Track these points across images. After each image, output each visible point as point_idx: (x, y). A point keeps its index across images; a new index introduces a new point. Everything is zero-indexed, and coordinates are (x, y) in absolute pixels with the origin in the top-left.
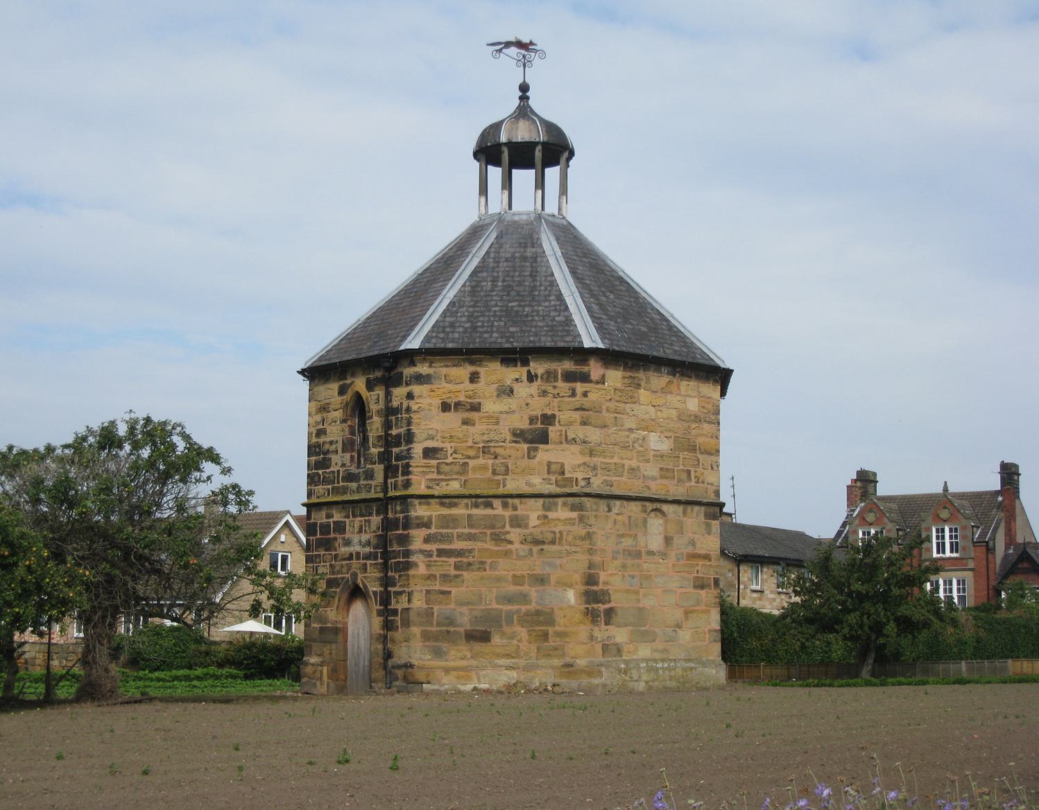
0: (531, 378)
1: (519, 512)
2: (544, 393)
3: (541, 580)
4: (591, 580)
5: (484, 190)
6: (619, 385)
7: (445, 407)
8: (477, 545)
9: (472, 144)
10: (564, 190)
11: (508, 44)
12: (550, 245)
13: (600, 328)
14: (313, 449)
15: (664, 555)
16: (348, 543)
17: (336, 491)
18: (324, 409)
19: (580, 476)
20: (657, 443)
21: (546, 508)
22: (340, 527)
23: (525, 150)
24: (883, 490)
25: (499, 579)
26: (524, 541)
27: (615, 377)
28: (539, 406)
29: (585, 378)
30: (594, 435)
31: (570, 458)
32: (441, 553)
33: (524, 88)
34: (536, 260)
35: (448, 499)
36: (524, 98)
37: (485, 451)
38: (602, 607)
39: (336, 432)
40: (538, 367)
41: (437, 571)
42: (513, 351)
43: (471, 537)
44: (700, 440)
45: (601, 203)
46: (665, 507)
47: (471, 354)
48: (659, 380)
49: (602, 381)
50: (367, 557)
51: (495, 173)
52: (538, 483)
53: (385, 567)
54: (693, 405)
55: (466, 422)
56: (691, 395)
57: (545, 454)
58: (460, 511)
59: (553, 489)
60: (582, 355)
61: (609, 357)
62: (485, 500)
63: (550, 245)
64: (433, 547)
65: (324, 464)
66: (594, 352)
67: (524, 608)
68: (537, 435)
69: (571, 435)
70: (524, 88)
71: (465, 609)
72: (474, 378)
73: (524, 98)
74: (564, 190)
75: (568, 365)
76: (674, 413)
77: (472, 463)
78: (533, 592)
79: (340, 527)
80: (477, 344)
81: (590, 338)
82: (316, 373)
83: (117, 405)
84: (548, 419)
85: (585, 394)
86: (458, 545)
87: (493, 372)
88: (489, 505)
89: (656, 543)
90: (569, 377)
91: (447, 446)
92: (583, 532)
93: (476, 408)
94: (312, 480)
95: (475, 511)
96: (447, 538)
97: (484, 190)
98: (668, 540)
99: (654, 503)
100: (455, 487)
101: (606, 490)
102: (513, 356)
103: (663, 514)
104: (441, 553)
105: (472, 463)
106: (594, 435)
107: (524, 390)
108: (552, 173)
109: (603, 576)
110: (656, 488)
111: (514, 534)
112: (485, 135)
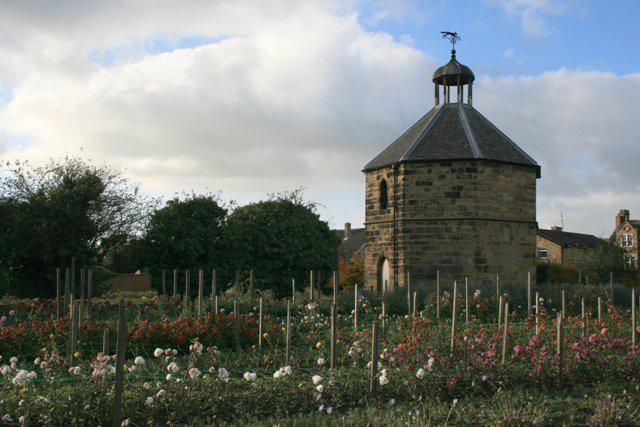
0: (453, 171)
1: (448, 226)
2: (458, 177)
3: (457, 254)
4: (478, 254)
5: (437, 95)
6: (490, 173)
7: (418, 184)
8: (431, 240)
9: (431, 78)
10: (470, 94)
11: (448, 33)
12: (463, 116)
13: (481, 147)
14: (368, 202)
15: (510, 243)
16: (381, 239)
17: (376, 218)
18: (371, 185)
19: (474, 211)
20: (508, 197)
21: (459, 224)
22: (378, 233)
23: (456, 76)
24: (352, 227)
25: (440, 254)
26: (450, 238)
27: (488, 170)
28: (456, 182)
29: (475, 171)
30: (479, 194)
31: (469, 204)
32: (416, 243)
33: (454, 52)
34: (457, 122)
35: (419, 222)
36: (454, 57)
37: (434, 201)
38: (483, 265)
39: (377, 195)
40: (456, 166)
41: (414, 250)
42: (445, 160)
43: (429, 237)
44: (527, 196)
45: (488, 99)
46: (511, 224)
47: (429, 162)
48: (509, 170)
49: (483, 172)
50: (388, 244)
51: (441, 87)
52: (456, 214)
53: (395, 249)
54: (523, 181)
55: (426, 190)
56: (521, 178)
57: (459, 202)
58: (423, 226)
59: (462, 217)
60: (473, 160)
61: (486, 162)
62: (430, 221)
63: (463, 116)
64: (413, 241)
65: (372, 207)
66: (479, 159)
67: (450, 265)
68: (455, 194)
69: (470, 194)
70: (454, 52)
71: (425, 266)
72: (429, 172)
73: (454, 57)
74: (470, 94)
75: (468, 165)
76: (514, 185)
77: (429, 206)
78: (454, 259)
79: (378, 233)
80: (431, 158)
81: (477, 153)
82: (368, 171)
83: (201, 192)
84: (460, 188)
85: (475, 178)
86: (423, 240)
87: (437, 169)
88: (436, 223)
89: (506, 238)
90: (468, 170)
91: (419, 199)
92: (474, 234)
93: (430, 184)
94: (367, 214)
95: (431, 226)
96: (419, 237)
97: (437, 95)
98: (512, 237)
99: (506, 222)
100: (421, 216)
101: (485, 217)
102: (445, 163)
103: (509, 227)
104: (416, 243)
105: (429, 206)
106: (479, 194)
107: (450, 176)
108: (466, 87)
109: (483, 252)
110: (507, 216)
111: (446, 235)
112: (436, 73)
